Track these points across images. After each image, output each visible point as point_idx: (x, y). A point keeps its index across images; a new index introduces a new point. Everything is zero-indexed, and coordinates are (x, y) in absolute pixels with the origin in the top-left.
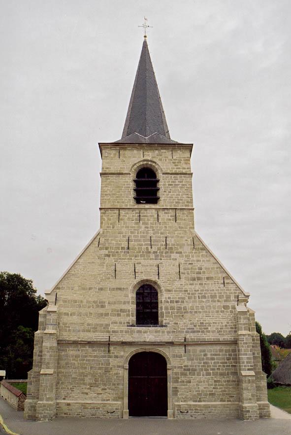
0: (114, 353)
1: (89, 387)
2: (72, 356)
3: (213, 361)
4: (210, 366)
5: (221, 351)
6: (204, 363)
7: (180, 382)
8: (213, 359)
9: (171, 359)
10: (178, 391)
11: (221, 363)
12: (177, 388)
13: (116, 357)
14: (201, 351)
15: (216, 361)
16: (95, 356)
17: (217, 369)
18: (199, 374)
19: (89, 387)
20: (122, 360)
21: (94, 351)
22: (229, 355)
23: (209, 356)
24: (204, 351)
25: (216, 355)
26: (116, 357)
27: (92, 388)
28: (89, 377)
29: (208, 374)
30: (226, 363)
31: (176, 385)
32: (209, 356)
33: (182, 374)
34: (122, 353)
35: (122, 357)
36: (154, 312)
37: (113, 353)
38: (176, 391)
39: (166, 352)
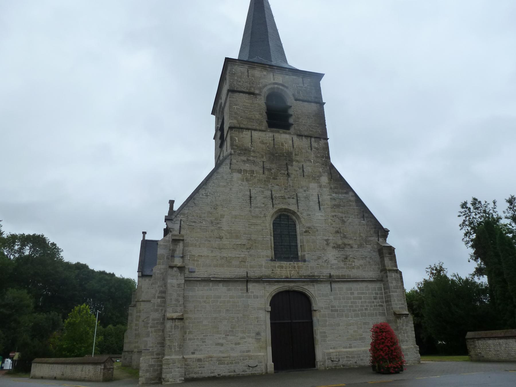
1: (224, 336)
3: (360, 301)
6: (352, 303)
8: (360, 298)
12: (325, 332)
18: (347, 316)
21: (229, 290)
23: (356, 295)
25: (362, 293)
29: (357, 316)
30: (373, 302)
32: (356, 295)
37: (252, 292)
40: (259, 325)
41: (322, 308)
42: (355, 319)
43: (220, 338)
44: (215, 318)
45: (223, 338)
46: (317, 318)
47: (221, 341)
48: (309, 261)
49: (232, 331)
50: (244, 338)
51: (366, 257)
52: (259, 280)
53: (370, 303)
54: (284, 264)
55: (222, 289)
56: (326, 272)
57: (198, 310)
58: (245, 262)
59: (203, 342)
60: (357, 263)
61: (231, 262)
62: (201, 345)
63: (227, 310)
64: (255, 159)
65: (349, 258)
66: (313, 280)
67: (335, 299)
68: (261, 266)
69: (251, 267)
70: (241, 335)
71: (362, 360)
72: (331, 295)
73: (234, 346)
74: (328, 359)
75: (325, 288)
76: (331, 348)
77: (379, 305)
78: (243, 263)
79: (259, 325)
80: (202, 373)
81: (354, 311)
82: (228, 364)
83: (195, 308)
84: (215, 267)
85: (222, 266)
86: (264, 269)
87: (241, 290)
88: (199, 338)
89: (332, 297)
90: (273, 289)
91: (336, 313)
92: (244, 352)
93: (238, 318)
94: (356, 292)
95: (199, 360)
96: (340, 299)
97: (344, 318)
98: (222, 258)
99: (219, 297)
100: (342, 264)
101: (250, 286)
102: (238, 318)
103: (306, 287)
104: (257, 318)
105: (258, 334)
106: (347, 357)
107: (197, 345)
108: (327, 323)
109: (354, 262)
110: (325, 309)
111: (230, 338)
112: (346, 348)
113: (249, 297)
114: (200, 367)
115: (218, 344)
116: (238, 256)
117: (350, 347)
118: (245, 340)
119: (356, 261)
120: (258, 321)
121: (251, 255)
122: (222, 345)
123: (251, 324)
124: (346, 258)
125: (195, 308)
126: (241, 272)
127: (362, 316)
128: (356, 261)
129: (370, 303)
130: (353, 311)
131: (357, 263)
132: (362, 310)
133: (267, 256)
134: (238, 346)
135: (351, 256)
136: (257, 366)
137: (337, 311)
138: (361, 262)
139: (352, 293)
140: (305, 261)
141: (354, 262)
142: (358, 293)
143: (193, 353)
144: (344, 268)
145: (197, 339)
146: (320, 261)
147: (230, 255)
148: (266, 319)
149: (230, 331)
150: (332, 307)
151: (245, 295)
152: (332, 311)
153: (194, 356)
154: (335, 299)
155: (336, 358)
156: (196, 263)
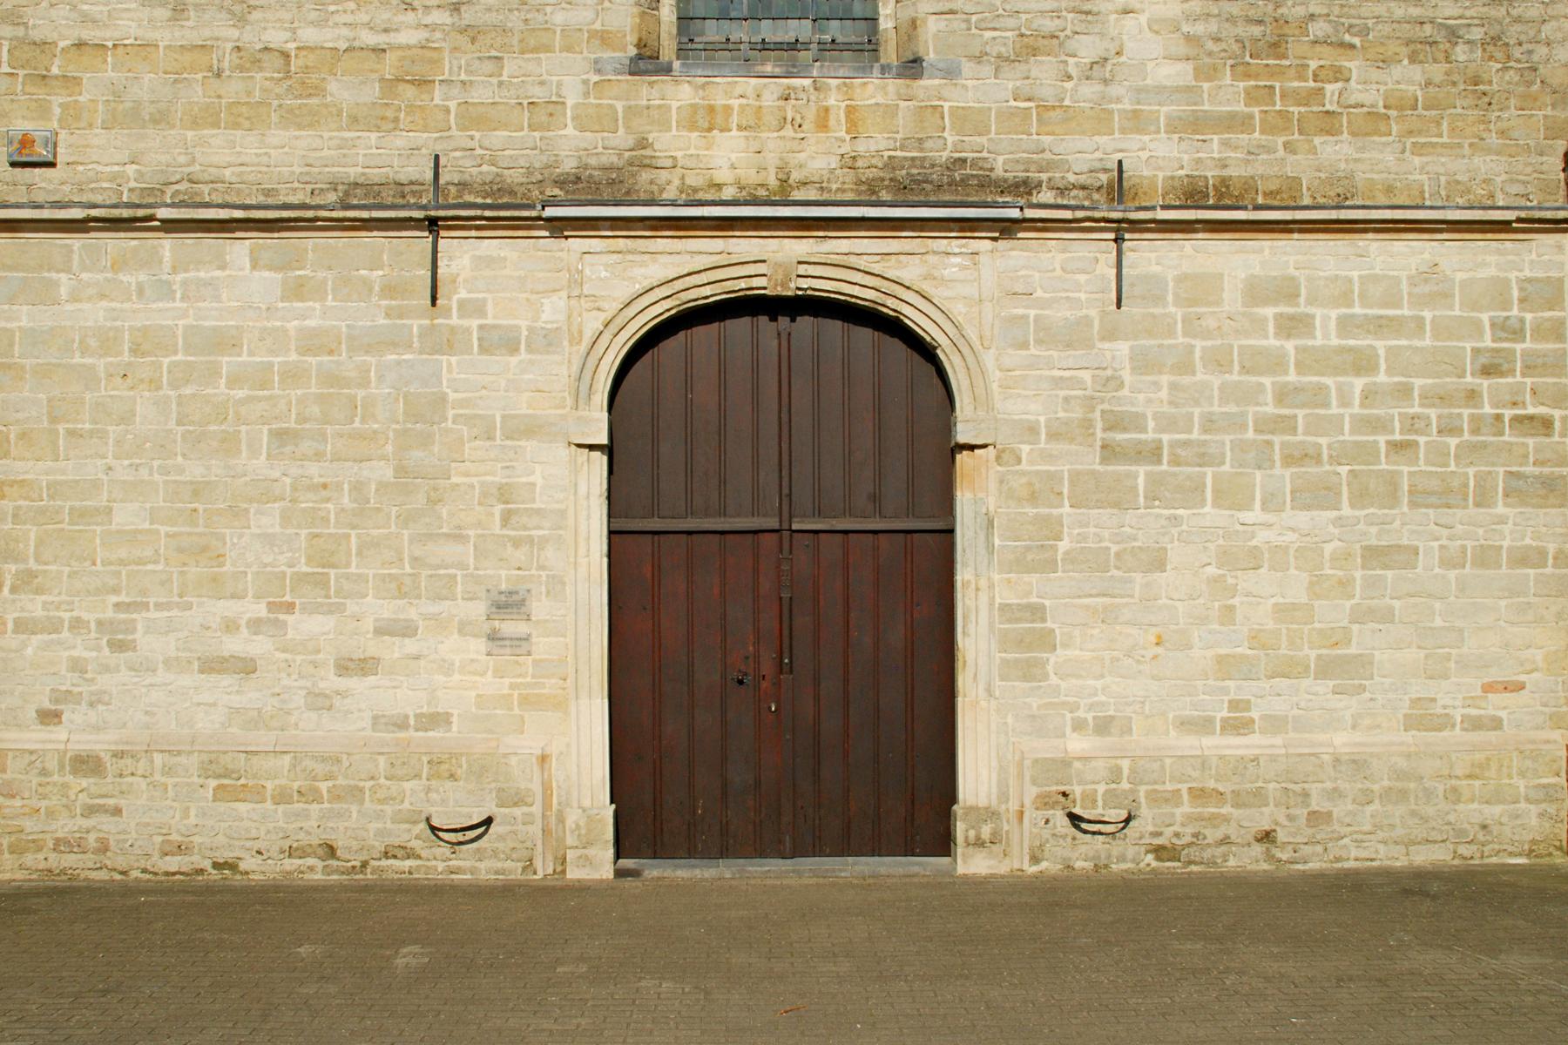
0: (478, 309)
1: (261, 610)
2: (107, 341)
3: (1359, 383)
4: (1336, 423)
5: (1433, 288)
6: (1282, 396)
7: (1070, 557)
8: (1362, 363)
9: (989, 359)
10: (1046, 641)
11: (1427, 398)
12: (1037, 612)
13: (501, 342)
14: (1256, 292)
15: (1382, 378)
16: (313, 343)
17: (1396, 447)
18: (1231, 496)
19: (261, 610)
20: (559, 368)
21: (297, 291)
22: (1500, 327)
23: (1326, 335)
24: (1286, 290)
25: (1380, 326)
26: (501, 342)
27: (290, 619)
28: (268, 520)
29: (1317, 495)
30: (1472, 396)
31: (1034, 588)
32: (1326, 335)
33: (1089, 493)
34: (552, 310)
35: (546, 341)
36: (978, 884)
37: (473, 308)
38: (1030, 636)
39: (941, 284)
40: (517, 542)
41: (1033, 429)
42: (1303, 519)
43: (230, 626)
44: (198, 490)
45: (256, 625)
46: (978, 497)
47: (234, 645)
48: (951, 73)
49: (322, 582)
50: (408, 630)
51: (1453, 35)
52: (508, 213)
53: (1443, 399)
54: (738, 91)
55: (927, 536)
56: (1082, 155)
57: (71, 433)
58: (423, 83)
59: (119, 646)
60: (1365, 85)
61: (319, 91)
62: (106, 669)
63: (281, 436)
64: (838, 118)
65: (1295, 48)
66: (981, 205)
67: (1144, 364)
68: (546, 111)
69: (474, 118)
70: (376, 608)
71: (1315, 818)
72: (1110, 335)
73: (331, 681)
74: (1044, 802)
75: (1067, 269)
76: (1079, 726)
77: (1517, 420)
78: (409, 92)
79: (517, 542)
80: (103, 848)
81: (1298, 457)
82: (282, 798)
83: (54, 420)
84: (195, 124)
85: (245, 116)
86: (570, 130)
87: (390, 290)
88: (90, 617)
89: (1123, 348)
90: (639, 279)
91: (1142, 471)
92: (402, 724)
93: (358, 487)
94: (1326, 319)
95: (86, 764)
96: (1186, 367)
97: (1209, 511)
98: (250, 59)
99: (226, 342)
100: (1228, 95)
101: (462, 255)
102: (358, 487)
103: (909, 271)
104: (504, 493)
105: (509, 604)
106: (1199, 794)
107: (77, 666)
108: (1063, 545)
109: (1339, 75)
110: (1053, 436)
111: (303, 625)
112: (1202, 725)
113: (449, 343)
114: (90, 811)
115: (213, 665)
116: (370, 39)
117: (1238, 726)
118: (411, 645)
119: (1354, 65)
120: (506, 518)
121: (473, 33)
122: (247, 667)
123: (458, 537)
124: (1276, 47)
125: (54, 420)
126: (393, 156)
127: (1361, 497)
128: (1354, 65)
129: (1443, 399)
130: (1289, 460)
131: (1365, 85)
132: (1365, 453)
133: (604, 38)
134: (353, 683)
135: (1318, 29)
136: (488, 822)
137: (1153, 453)
138: (1407, 77)
139: (1293, 325)
140: (913, 66)
141: (1339, 75)
142: (1345, 325)
143: (49, 717)
144: (1245, 124)
145: (77, 624)
146: (1043, 70)
147: (309, 35)
148: (572, 505)
149: (301, 578)
150: (1115, 422)
151: (416, 325)
152: (1110, 452)
153: (58, 736)
154: (1144, 364)
155: (1112, 798)
156: (57, 101)
